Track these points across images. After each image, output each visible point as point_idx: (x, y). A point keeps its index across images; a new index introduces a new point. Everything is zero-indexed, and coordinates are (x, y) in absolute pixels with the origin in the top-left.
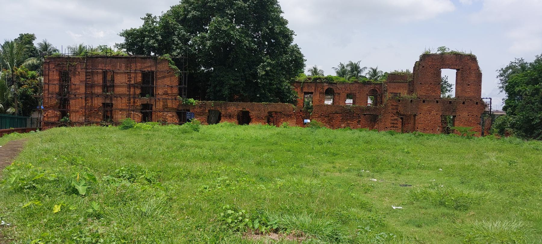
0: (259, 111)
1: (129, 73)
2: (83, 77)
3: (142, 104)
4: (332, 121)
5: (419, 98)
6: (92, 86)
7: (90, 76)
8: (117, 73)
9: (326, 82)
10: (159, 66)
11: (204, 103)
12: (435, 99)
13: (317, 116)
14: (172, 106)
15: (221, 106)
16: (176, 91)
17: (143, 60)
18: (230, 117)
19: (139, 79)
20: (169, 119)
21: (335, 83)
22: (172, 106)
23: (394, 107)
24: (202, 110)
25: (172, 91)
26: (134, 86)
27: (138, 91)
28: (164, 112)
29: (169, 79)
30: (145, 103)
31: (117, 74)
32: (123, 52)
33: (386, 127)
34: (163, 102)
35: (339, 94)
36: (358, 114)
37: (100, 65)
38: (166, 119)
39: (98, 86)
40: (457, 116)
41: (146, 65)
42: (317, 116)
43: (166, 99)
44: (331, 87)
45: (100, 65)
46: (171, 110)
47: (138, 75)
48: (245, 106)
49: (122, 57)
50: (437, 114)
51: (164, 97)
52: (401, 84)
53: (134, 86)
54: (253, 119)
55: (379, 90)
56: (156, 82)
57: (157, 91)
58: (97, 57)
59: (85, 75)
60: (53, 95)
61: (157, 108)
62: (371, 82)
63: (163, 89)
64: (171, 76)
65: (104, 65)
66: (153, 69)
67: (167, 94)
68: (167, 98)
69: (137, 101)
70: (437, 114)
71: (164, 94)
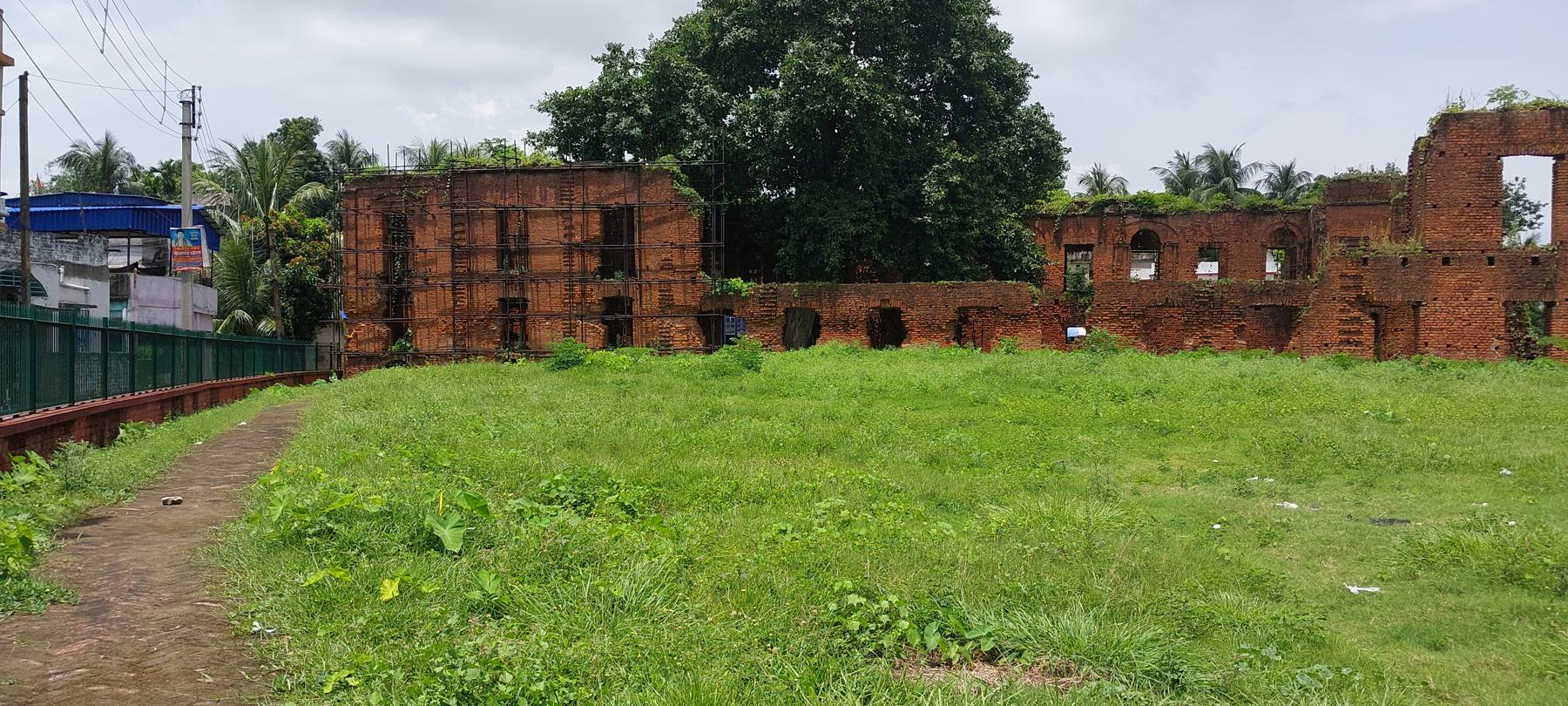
3: (606, 300)
4: (1155, 330)
5: (1430, 252)
9: (1133, 212)
10: (646, 190)
12: (1483, 251)
13: (1106, 315)
14: (685, 302)
16: (693, 257)
17: (605, 177)
19: (595, 229)
20: (678, 337)
21: (1160, 215)
22: (685, 302)
23: (1350, 283)
25: (682, 256)
26: (582, 249)
27: (593, 263)
29: (674, 225)
30: (613, 294)
33: (1326, 345)
34: (660, 291)
35: (1174, 246)
36: (1237, 307)
40: (1558, 304)
41: (612, 189)
42: (1106, 315)
43: (669, 282)
44: (1150, 226)
46: (681, 312)
47: (590, 219)
48: (887, 294)
50: (1490, 299)
51: (663, 275)
52: (1372, 211)
53: (582, 249)
54: (912, 330)
56: (640, 234)
57: (643, 262)
61: (644, 307)
62: (1275, 206)
63: (659, 254)
64: (682, 216)
66: (632, 199)
67: (670, 269)
69: (592, 290)
70: (1490, 299)
71: (662, 268)
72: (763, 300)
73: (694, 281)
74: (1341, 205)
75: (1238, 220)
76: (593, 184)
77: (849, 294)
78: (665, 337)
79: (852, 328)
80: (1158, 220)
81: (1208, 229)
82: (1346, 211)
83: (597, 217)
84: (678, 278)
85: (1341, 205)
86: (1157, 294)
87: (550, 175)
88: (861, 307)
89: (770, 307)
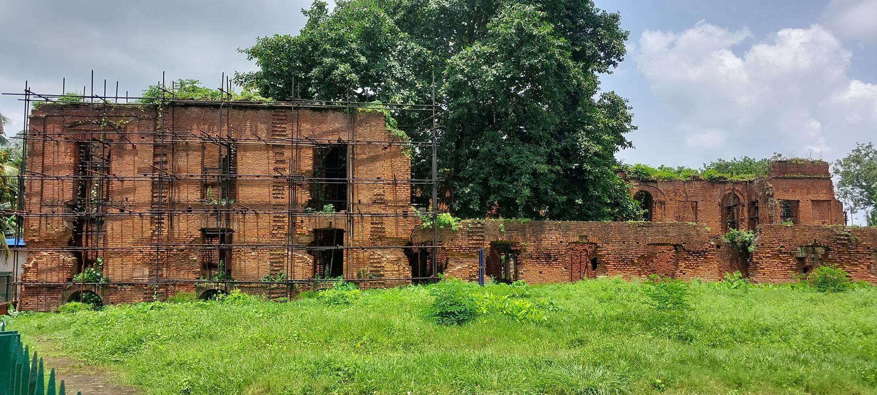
0: (624, 243)
1: (277, 149)
2: (146, 158)
4: (652, 261)
6: (173, 182)
7: (165, 155)
8: (246, 148)
9: (634, 178)
11: (479, 225)
14: (397, 234)
15: (522, 230)
16: (404, 193)
18: (548, 258)
20: (389, 267)
22: (397, 234)
24: (474, 242)
28: (374, 250)
29: (387, 164)
31: (245, 151)
32: (255, 94)
34: (372, 224)
35: (662, 203)
36: (868, 248)
37: (195, 127)
38: (380, 267)
39: (189, 181)
41: (325, 127)
44: (646, 189)
45: (195, 127)
47: (302, 155)
49: (256, 107)
51: (375, 209)
52: (800, 183)
55: (742, 195)
57: (355, 196)
58: (187, 106)
59: (152, 154)
60: (55, 209)
61: (355, 238)
64: (394, 155)
65: (206, 127)
67: (381, 203)
68: (383, 212)
71: (375, 202)
72: (470, 233)
73: (405, 215)
74: (781, 178)
75: (703, 187)
76: (307, 122)
77: (551, 230)
78: (377, 267)
79: (553, 261)
80: (651, 184)
81: (684, 191)
82: (784, 182)
83: (310, 153)
84: (390, 211)
85: (781, 178)
86: (807, 236)
87: (262, 111)
88: (561, 242)
89: (477, 240)
